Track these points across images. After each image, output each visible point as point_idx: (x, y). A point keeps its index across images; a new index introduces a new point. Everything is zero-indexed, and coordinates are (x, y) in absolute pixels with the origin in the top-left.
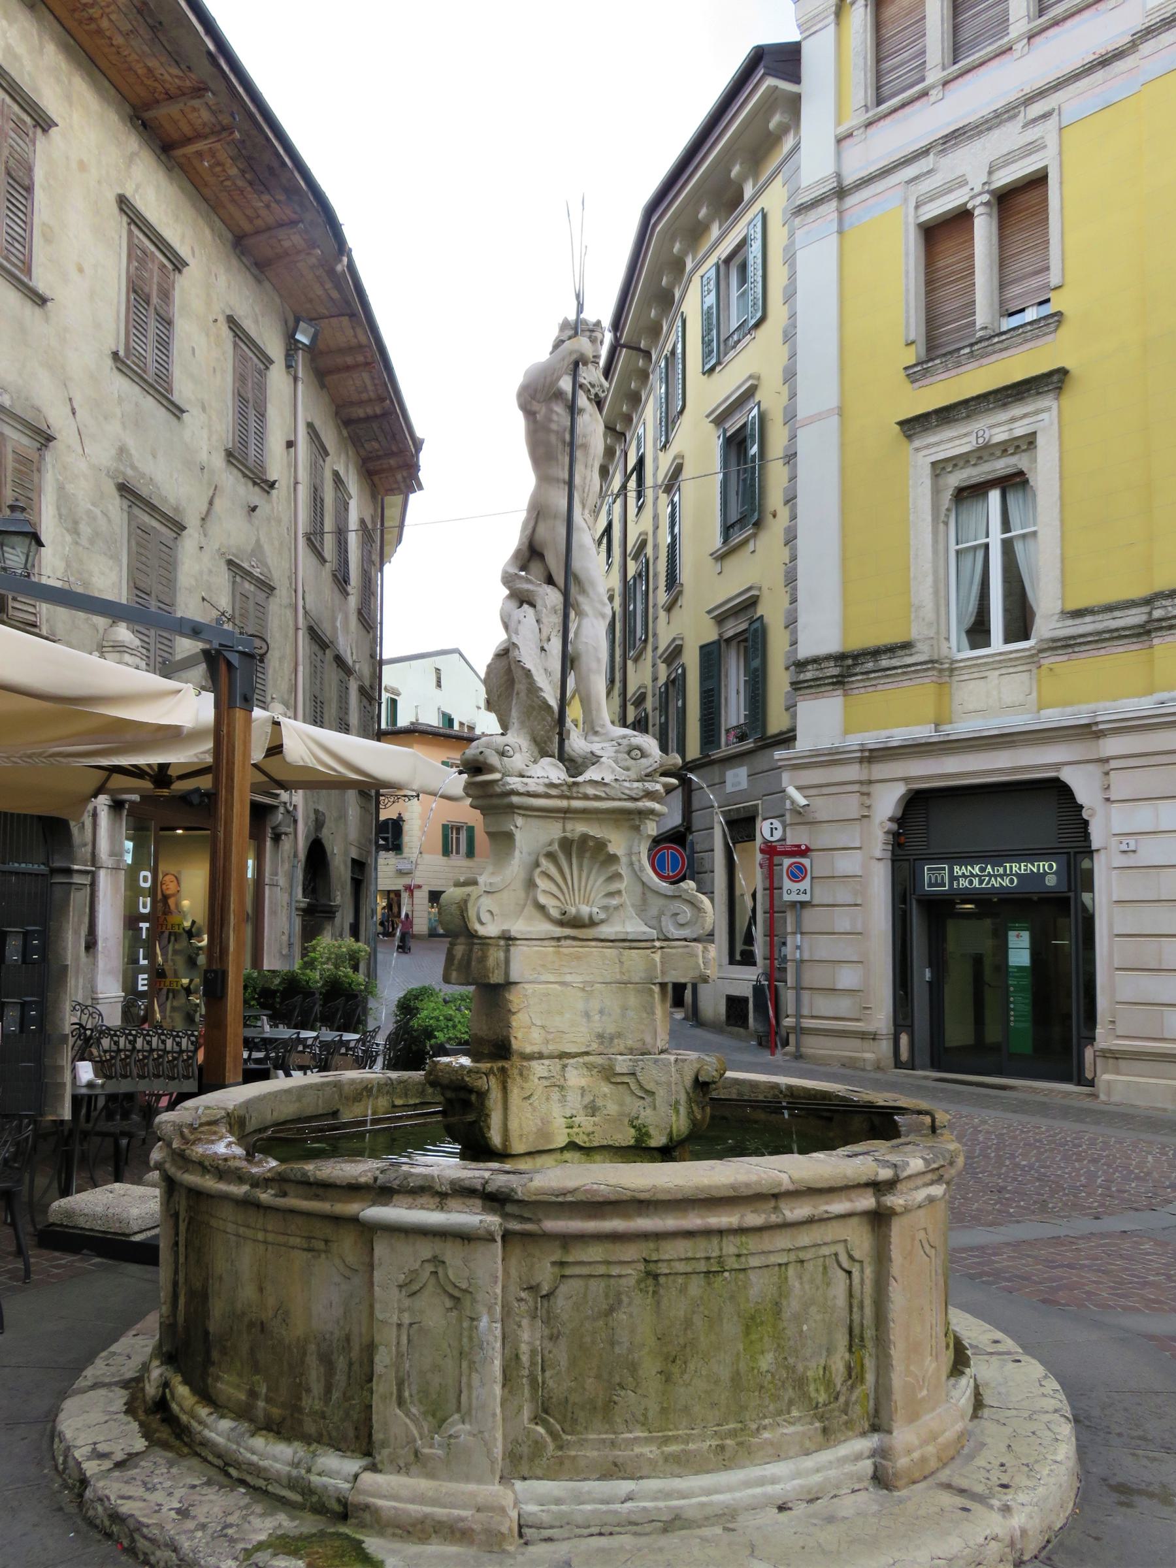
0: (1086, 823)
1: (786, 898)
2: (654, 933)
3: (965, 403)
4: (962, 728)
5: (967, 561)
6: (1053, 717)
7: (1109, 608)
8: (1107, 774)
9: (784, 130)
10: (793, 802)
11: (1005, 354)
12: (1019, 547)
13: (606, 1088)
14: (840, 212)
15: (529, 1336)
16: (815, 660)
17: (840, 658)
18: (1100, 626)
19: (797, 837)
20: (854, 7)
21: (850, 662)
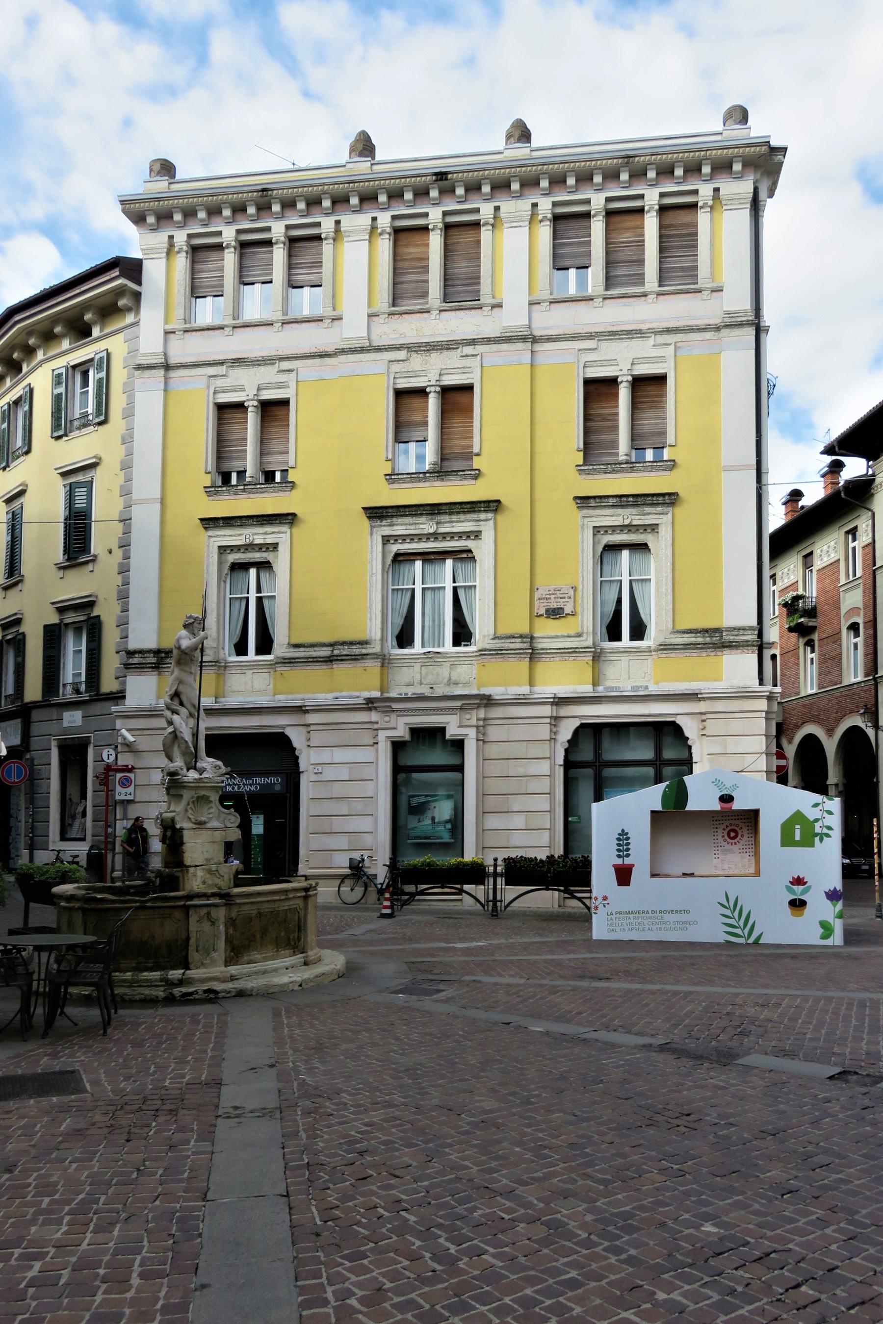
0: (297, 758)
1: (118, 798)
2: (222, 826)
3: (240, 518)
4: (233, 701)
5: (236, 604)
6: (282, 700)
7: (313, 645)
8: (309, 732)
9: (129, 310)
10: (125, 739)
11: (262, 495)
12: (266, 603)
13: (208, 876)
14: (166, 379)
15: (231, 931)
16: (141, 652)
17: (157, 652)
18: (308, 654)
19: (125, 760)
20: (179, 255)
21: (163, 655)
